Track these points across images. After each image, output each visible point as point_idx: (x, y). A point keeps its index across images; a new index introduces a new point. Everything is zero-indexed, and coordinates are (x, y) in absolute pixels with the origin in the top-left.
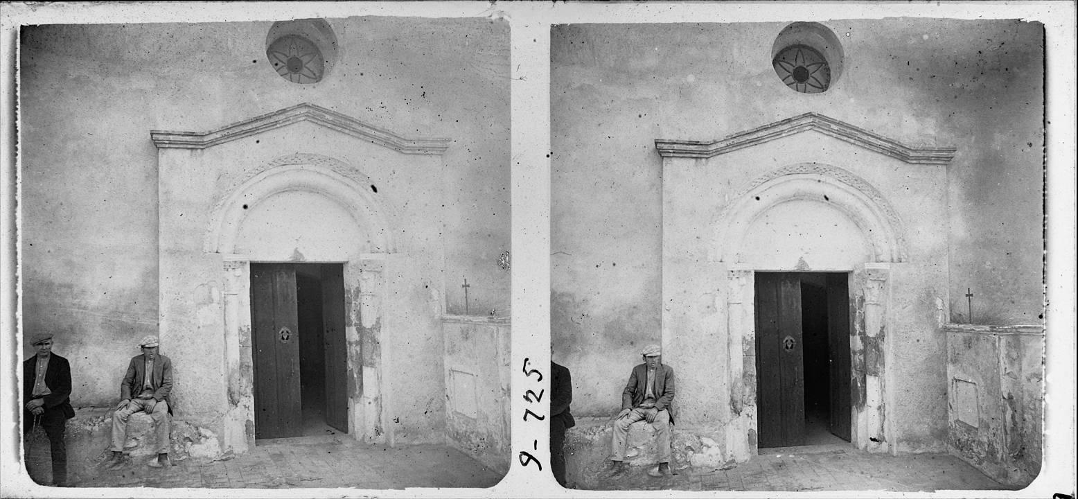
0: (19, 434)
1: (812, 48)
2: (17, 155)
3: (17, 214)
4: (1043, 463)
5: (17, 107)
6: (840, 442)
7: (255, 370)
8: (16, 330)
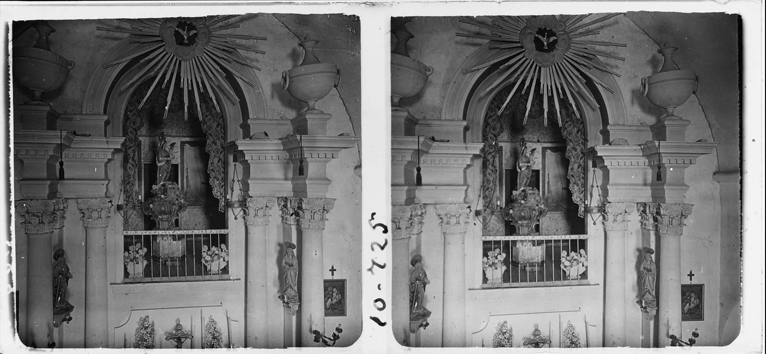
0: (14, 312)
1: (11, 260)
2: (9, 115)
3: (12, 276)
4: (742, 326)
5: (9, 81)
6: (66, 255)
7: (116, 24)
8: (13, 304)
